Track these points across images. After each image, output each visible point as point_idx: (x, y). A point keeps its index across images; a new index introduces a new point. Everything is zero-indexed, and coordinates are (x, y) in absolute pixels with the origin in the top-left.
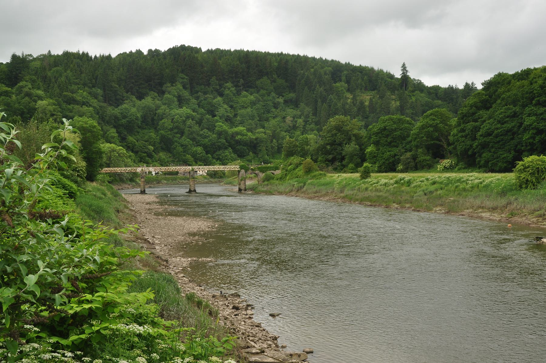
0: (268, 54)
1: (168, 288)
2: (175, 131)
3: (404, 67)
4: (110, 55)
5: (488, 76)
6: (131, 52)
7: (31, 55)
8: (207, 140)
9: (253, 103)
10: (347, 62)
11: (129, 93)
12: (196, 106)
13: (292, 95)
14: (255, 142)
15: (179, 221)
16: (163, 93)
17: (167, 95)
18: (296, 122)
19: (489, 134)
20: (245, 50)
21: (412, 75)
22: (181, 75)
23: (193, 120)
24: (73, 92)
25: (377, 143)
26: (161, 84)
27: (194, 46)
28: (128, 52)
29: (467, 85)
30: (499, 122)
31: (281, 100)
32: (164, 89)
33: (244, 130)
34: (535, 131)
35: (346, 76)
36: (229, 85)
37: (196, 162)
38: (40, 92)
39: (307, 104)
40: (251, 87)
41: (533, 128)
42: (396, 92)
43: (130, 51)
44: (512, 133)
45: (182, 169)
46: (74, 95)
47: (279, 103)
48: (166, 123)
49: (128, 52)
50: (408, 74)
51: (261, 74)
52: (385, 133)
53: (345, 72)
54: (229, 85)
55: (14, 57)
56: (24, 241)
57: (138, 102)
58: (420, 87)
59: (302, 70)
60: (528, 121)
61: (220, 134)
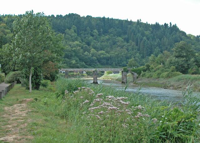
12: (81, 41)
22: (74, 26)
54: (95, 31)
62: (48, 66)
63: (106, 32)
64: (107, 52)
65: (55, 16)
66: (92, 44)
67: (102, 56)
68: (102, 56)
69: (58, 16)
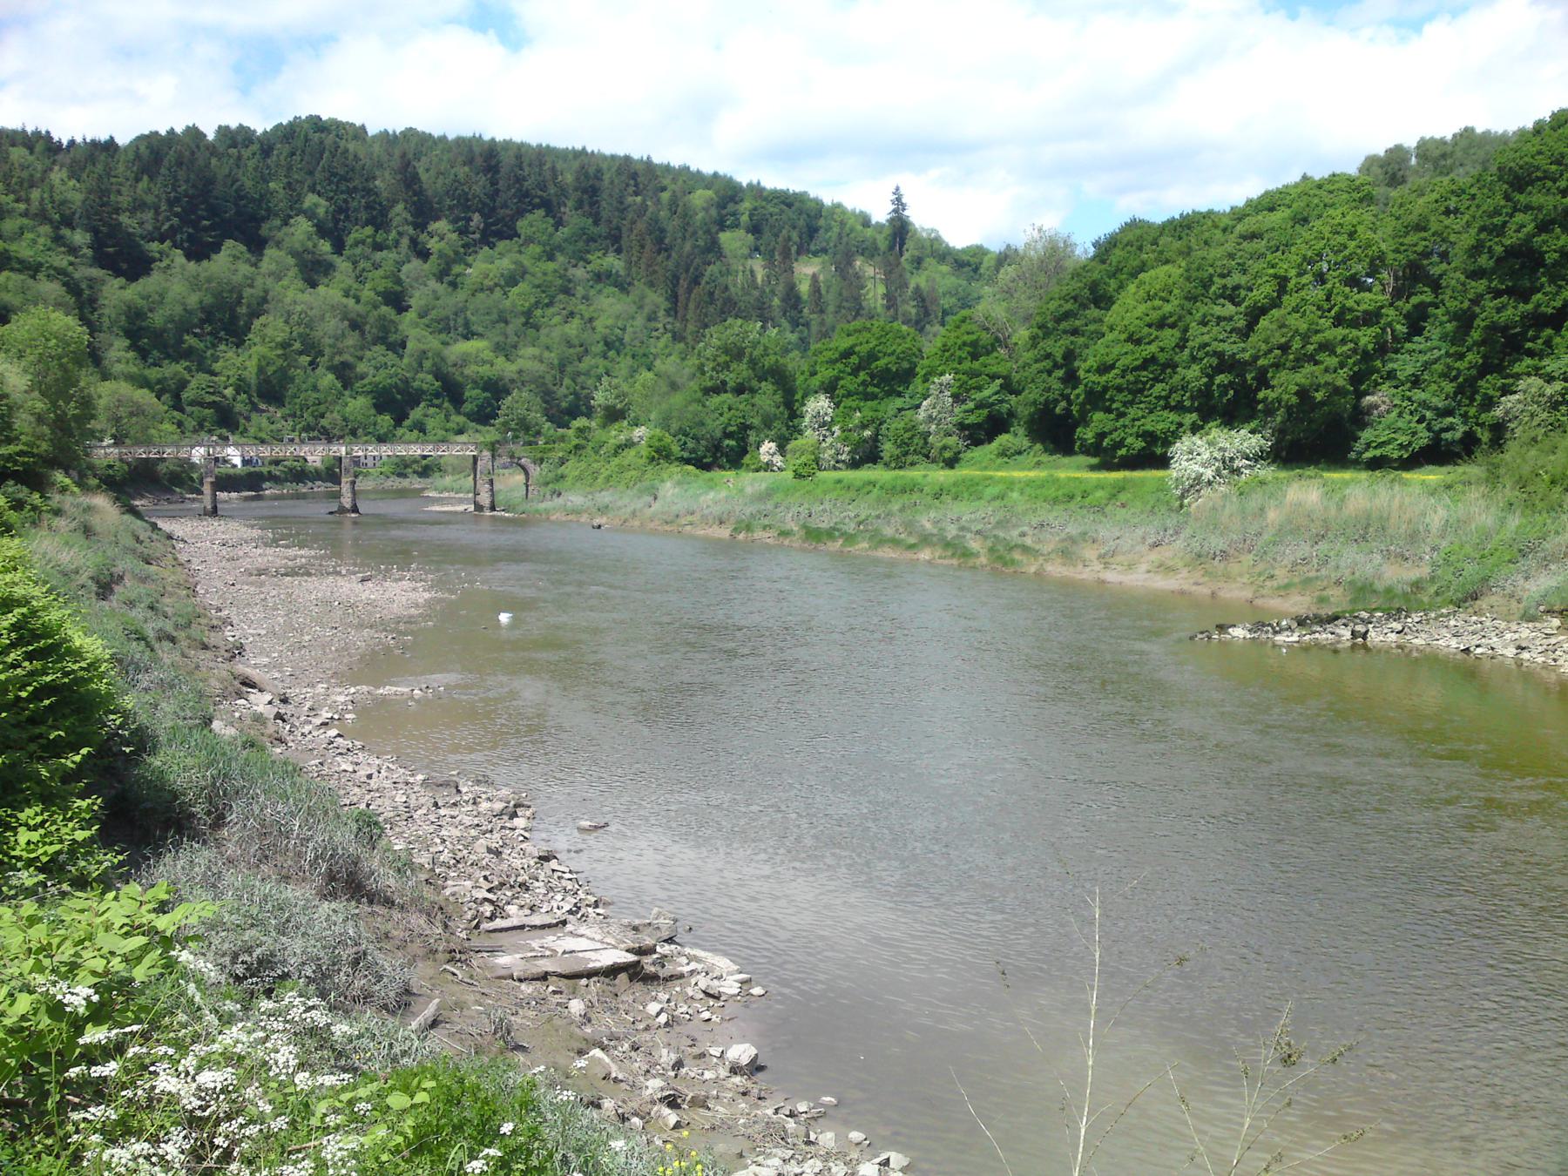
0: (549, 151)
1: (38, 1156)
3: (898, 201)
4: (112, 138)
5: (1109, 225)
6: (171, 132)
11: (168, 243)
13: (613, 262)
15: (312, 583)
17: (270, 252)
19: (1104, 369)
20: (487, 137)
26: (258, 220)
27: (344, 120)
28: (163, 133)
30: (1130, 339)
31: (579, 273)
34: (1214, 361)
35: (751, 216)
36: (441, 226)
40: (501, 236)
43: (168, 128)
45: (316, 455)
48: (271, 329)
49: (163, 133)
50: (906, 213)
51: (527, 201)
53: (747, 205)
56: (77, 1100)
57: (192, 265)
58: (938, 251)
59: (636, 194)
60: (1198, 335)
63: (498, 230)
65: (211, 136)
69: (223, 131)
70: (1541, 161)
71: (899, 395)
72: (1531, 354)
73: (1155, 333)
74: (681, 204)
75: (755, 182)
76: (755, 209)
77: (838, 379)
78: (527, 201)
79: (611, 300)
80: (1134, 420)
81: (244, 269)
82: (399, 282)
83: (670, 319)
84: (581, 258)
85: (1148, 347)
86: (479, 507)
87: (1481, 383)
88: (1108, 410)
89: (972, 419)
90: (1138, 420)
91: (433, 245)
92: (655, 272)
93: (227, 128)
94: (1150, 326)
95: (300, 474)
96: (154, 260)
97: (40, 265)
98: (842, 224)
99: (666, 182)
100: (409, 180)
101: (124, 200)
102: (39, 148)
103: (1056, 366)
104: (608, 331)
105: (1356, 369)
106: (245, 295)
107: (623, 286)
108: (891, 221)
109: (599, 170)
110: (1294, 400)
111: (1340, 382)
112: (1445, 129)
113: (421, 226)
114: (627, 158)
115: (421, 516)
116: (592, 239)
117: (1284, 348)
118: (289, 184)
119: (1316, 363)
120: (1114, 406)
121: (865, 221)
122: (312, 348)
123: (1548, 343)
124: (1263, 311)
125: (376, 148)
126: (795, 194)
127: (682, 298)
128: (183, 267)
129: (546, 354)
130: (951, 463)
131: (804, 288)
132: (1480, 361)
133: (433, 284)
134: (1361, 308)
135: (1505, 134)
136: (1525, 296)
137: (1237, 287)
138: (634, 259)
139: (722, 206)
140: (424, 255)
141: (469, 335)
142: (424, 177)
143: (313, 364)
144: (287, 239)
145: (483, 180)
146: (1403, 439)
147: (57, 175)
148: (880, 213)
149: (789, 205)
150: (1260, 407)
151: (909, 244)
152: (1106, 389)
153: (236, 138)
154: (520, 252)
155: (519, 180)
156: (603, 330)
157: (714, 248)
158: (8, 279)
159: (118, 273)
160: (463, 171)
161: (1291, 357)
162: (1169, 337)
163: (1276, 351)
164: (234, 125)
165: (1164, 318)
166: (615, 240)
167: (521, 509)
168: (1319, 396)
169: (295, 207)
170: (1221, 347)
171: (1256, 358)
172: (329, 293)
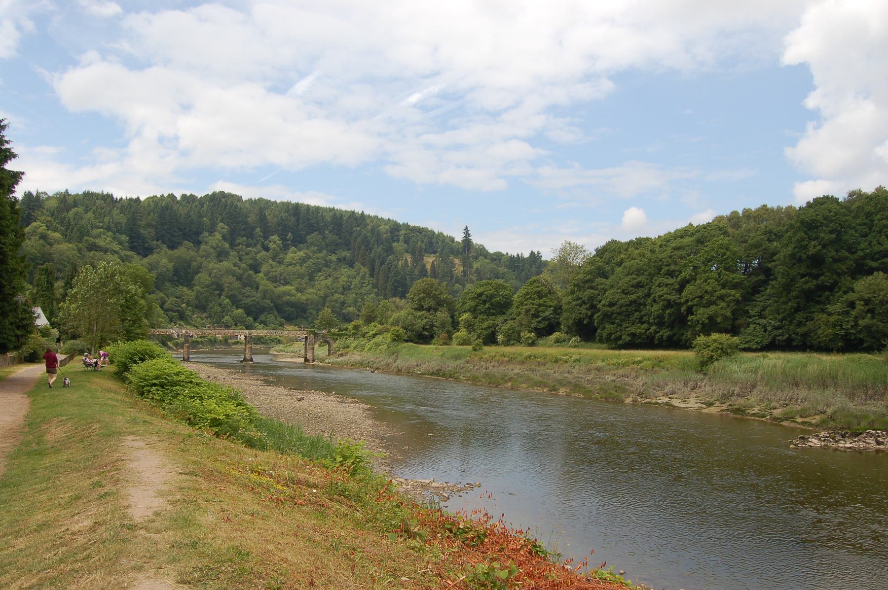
2: (214, 287)
5: (601, 242)
7: (45, 193)
8: (250, 299)
9: (303, 261)
10: (406, 223)
11: (160, 241)
12: (237, 260)
13: (347, 254)
14: (305, 302)
16: (199, 243)
17: (203, 247)
18: (351, 282)
19: (611, 305)
21: (476, 240)
22: (221, 224)
23: (233, 276)
24: (95, 237)
25: (473, 310)
26: (198, 233)
28: (159, 196)
29: (532, 253)
30: (623, 292)
31: (334, 258)
32: (200, 239)
33: (292, 289)
36: (275, 238)
37: (236, 325)
38: (57, 235)
39: (364, 265)
40: (300, 243)
41: (663, 300)
42: (459, 256)
44: (637, 305)
45: (219, 333)
46: (97, 241)
47: (331, 262)
48: (203, 278)
49: (159, 196)
50: (470, 238)
51: (312, 228)
52: (484, 298)
53: (403, 232)
54: (275, 238)
55: (191, 194)
57: (170, 252)
58: (482, 252)
60: (658, 292)
61: (265, 292)
62: (462, 333)
63: (298, 241)
64: (298, 290)
65: (179, 198)
66: (264, 268)
67: (288, 297)
68: (288, 297)
69: (184, 196)
70: (820, 218)
71: (504, 313)
72: (818, 302)
73: (634, 290)
74: (376, 230)
75: (406, 223)
76: (406, 234)
77: (476, 306)
78: (312, 228)
79: (346, 270)
80: (626, 328)
81: (193, 253)
82: (256, 260)
83: (371, 279)
84: (333, 252)
85: (631, 296)
86: (306, 360)
87: (796, 315)
88: (613, 323)
89: (542, 326)
90: (628, 328)
91: (272, 246)
92: (365, 259)
93: (185, 195)
94: (632, 287)
95: (213, 342)
96: (154, 249)
97: (108, 249)
98: (443, 241)
99: (368, 222)
100: (262, 218)
101: (143, 223)
102: (108, 201)
103: (584, 303)
104: (344, 283)
105: (734, 308)
106: (192, 264)
107: (351, 265)
108: (463, 241)
109: (342, 216)
110: (707, 321)
111: (729, 314)
112: (754, 206)
113: (266, 238)
114: (353, 212)
115: (275, 364)
116: (337, 245)
117: (701, 297)
118: (212, 218)
119: (716, 305)
120: (616, 321)
121: (452, 240)
122: (220, 288)
123: (827, 298)
124: (688, 282)
125: (247, 205)
126: (423, 228)
127: (376, 270)
128: (166, 252)
129: (319, 292)
130: (533, 344)
131: (428, 267)
132: (796, 305)
133: (271, 262)
134: (735, 281)
135: (779, 209)
136: (816, 277)
137: (674, 271)
138: (356, 253)
139: (392, 232)
140: (267, 249)
141: (286, 283)
142: (268, 217)
143: (220, 295)
144: (210, 242)
145: (293, 219)
146: (758, 340)
147: (115, 212)
148: (459, 238)
149: (421, 233)
150: (689, 323)
151: (472, 250)
152: (612, 314)
153: (189, 199)
154: (307, 249)
155: (308, 220)
156: (342, 283)
157: (390, 250)
158: (94, 254)
159: (139, 254)
160: (284, 215)
161: (704, 302)
162: (641, 293)
163: (697, 299)
164: (188, 194)
165: (638, 283)
166: (347, 245)
167: (327, 361)
168: (719, 320)
169: (212, 230)
170: (669, 297)
171: (687, 301)
172: (226, 264)
